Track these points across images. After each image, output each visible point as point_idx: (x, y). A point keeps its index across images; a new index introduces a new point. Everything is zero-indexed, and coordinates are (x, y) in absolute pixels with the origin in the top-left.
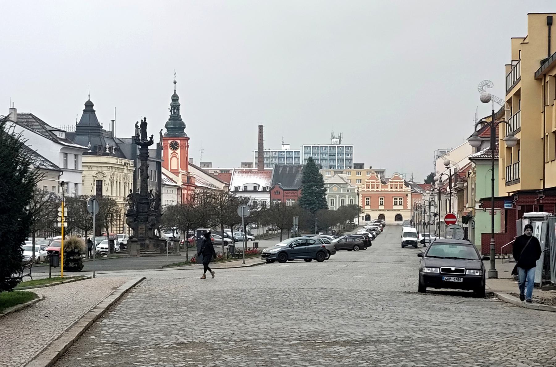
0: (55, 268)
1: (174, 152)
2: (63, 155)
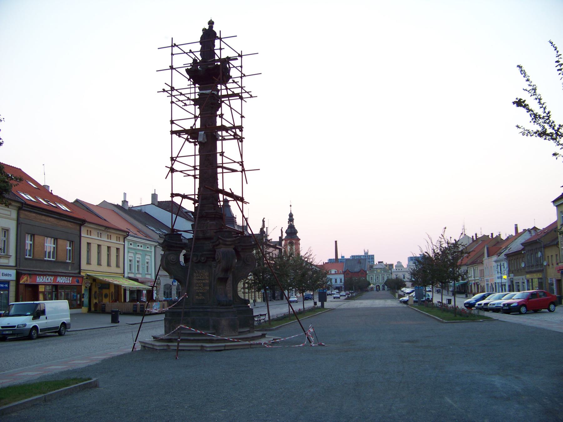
0: (115, 320)
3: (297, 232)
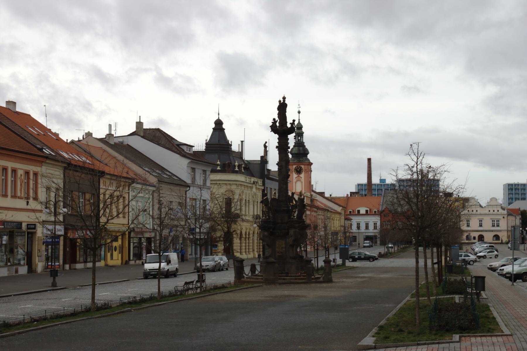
1: (298, 176)
2: (190, 171)
3: (308, 153)
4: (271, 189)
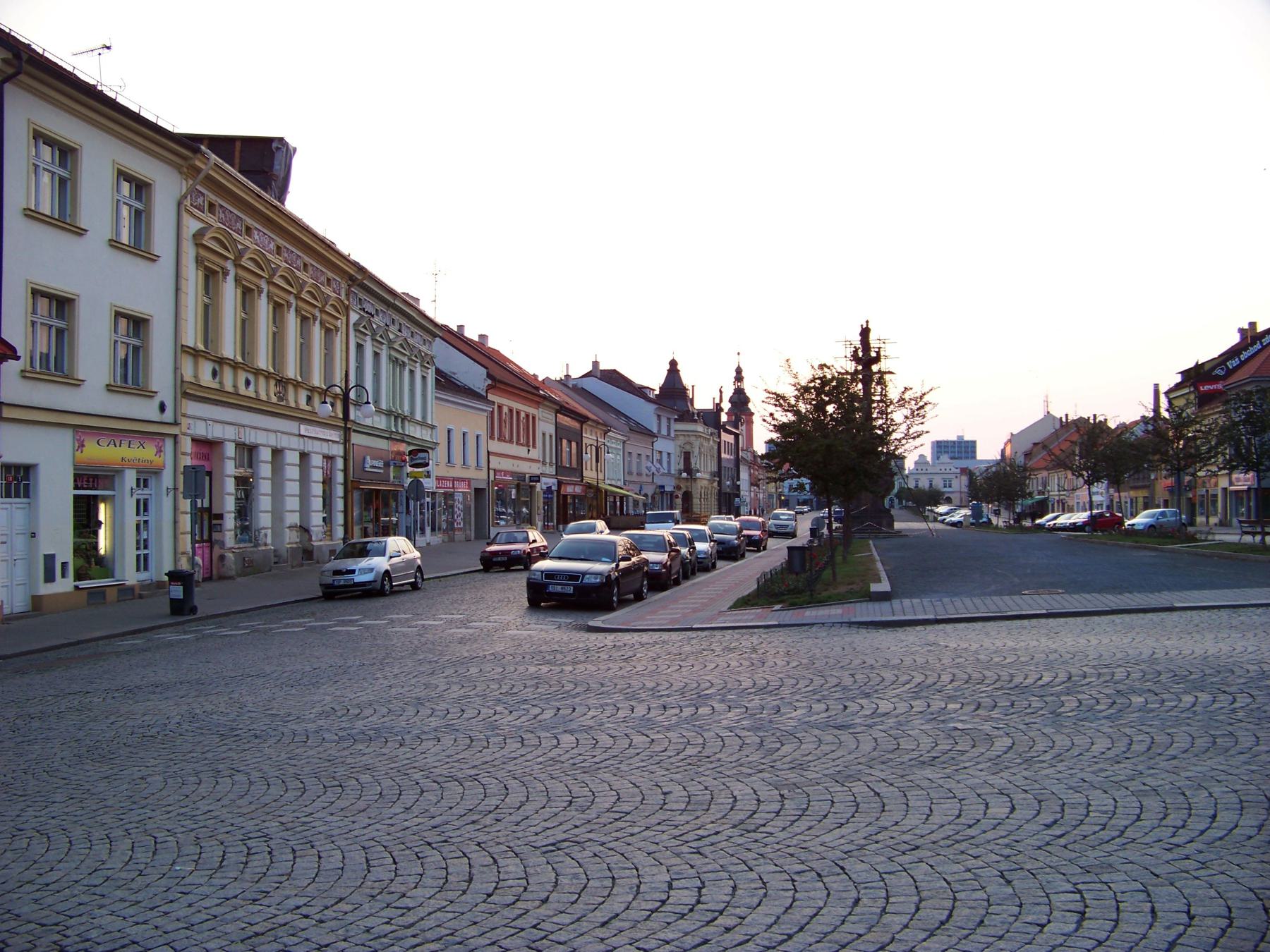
4: (669, 454)
